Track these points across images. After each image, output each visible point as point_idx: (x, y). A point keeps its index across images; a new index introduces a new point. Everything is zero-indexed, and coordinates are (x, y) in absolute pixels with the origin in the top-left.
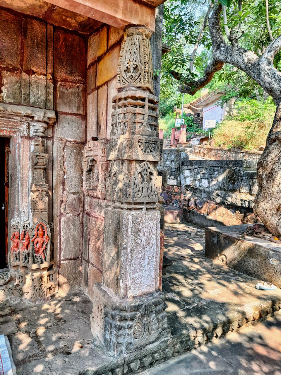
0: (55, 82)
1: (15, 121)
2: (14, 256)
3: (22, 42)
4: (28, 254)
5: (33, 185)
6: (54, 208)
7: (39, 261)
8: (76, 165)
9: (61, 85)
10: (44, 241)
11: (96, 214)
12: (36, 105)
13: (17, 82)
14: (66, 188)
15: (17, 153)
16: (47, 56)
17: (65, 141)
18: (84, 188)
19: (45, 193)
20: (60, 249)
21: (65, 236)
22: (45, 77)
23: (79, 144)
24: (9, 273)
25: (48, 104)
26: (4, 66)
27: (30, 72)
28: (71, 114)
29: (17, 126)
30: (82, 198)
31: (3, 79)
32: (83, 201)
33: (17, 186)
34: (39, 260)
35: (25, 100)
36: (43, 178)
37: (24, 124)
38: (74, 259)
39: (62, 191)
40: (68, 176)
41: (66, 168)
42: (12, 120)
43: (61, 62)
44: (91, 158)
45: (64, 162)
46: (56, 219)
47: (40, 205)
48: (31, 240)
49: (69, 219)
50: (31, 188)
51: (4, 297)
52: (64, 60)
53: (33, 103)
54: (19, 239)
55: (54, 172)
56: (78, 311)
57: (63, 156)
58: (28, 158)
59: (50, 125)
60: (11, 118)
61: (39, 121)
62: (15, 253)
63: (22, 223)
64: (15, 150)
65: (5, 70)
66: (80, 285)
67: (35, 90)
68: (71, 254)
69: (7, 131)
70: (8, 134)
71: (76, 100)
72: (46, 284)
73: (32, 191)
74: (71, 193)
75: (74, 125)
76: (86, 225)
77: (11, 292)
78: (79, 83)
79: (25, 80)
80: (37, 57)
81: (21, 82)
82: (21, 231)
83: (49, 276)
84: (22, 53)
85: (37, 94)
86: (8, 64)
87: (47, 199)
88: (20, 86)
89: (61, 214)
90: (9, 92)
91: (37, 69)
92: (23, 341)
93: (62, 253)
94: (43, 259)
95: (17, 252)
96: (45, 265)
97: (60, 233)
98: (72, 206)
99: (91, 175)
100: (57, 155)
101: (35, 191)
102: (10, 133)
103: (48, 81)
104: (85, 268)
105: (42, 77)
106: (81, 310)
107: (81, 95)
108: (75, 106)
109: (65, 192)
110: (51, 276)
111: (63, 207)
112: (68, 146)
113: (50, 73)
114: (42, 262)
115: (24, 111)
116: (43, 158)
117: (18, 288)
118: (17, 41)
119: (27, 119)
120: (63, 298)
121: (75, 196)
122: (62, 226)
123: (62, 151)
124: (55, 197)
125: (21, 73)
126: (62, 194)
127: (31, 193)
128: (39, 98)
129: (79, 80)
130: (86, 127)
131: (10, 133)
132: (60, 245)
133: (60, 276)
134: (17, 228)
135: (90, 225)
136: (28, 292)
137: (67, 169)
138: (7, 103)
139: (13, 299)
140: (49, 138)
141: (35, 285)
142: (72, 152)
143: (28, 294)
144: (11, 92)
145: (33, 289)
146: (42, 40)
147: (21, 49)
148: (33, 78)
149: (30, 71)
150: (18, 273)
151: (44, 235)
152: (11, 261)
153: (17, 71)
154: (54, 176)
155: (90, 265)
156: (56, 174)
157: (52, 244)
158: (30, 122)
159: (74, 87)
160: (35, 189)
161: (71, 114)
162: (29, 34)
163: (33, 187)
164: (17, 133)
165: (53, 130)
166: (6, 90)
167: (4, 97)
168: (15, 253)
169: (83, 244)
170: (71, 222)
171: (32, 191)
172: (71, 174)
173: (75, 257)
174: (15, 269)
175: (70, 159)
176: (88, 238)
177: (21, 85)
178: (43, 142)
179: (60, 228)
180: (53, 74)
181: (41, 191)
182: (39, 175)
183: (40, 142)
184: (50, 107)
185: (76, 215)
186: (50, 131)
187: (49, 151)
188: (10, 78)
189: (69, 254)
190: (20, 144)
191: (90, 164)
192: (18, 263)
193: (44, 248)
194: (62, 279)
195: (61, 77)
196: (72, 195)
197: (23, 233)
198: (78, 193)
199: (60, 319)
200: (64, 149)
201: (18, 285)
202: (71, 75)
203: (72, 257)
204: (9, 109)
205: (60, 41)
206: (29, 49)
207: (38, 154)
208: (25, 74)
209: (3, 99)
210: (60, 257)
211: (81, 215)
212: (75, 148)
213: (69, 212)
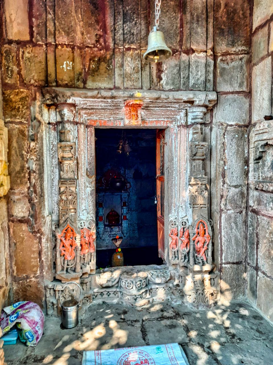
0: (215, 58)
1: (173, 109)
2: (173, 253)
3: (181, 20)
4: (188, 253)
5: (193, 178)
6: (212, 204)
7: (199, 263)
8: (238, 153)
9: (222, 60)
10: (205, 240)
11: (270, 212)
12: (196, 88)
14: (227, 180)
15: (174, 145)
16: (207, 29)
17: (225, 125)
18: (252, 179)
19: (204, 186)
20: (222, 250)
21: (226, 236)
22: (205, 53)
23: (241, 127)
24: (168, 271)
25: (208, 85)
27: (189, 51)
28: (232, 93)
29: (174, 115)
30: (245, 192)
32: (246, 196)
33: (174, 179)
34: (201, 261)
35: (184, 84)
36: (202, 170)
37: (182, 112)
38: (237, 263)
39: (222, 184)
40: (228, 167)
41: (227, 157)
42: (171, 108)
43: (222, 32)
44: (264, 143)
45: (224, 151)
46: (216, 216)
47: (199, 200)
48: (192, 239)
49: (230, 217)
50: (190, 181)
51: (165, 296)
52: (225, 30)
53: (193, 86)
54: (177, 235)
55: (212, 162)
56: (252, 329)
57: (223, 144)
58: (185, 148)
59: (210, 109)
60: (169, 107)
61: (199, 106)
62: (174, 250)
63: (180, 220)
64: (172, 141)
66: (244, 294)
67: (194, 72)
68: (234, 257)
69: (164, 121)
70: (165, 125)
71: (239, 76)
72: (209, 289)
73: (190, 184)
74: (232, 186)
75: (236, 106)
76: (252, 225)
77: (170, 291)
78: (242, 54)
79: (184, 62)
80: (196, 33)
81: (180, 65)
82: (179, 228)
83: (210, 279)
84: (182, 32)
85: (197, 75)
87: (207, 193)
88: (179, 70)
89: (222, 210)
91: (197, 46)
92: (199, 356)
93: (223, 255)
94: (205, 260)
95: (176, 250)
96: (207, 267)
97: (220, 233)
98: (233, 201)
99: (261, 163)
100: (217, 143)
101: (194, 185)
102: (167, 123)
103: (208, 58)
104: (252, 276)
105: (202, 55)
106: (255, 327)
107: (244, 67)
108: (237, 82)
109: (226, 185)
110: (212, 280)
111: (223, 202)
112: (228, 131)
113: (210, 49)
114: (203, 264)
115: (185, 96)
116: (202, 147)
117: (178, 288)
118: (177, 20)
119: (186, 105)
120: (227, 308)
121: (237, 190)
122: (222, 224)
123: (222, 137)
124: (213, 191)
125: (180, 54)
126: (222, 187)
127: (190, 187)
128: (198, 79)
129: (242, 50)
130: (250, 105)
131: (167, 123)
132: (221, 246)
133: (222, 281)
134: (175, 224)
135: (258, 226)
136: (190, 295)
137: (228, 157)
138: (166, 91)
139: (175, 300)
140: (207, 124)
141: (197, 288)
142: (233, 138)
143: (190, 297)
144: (170, 78)
145: (195, 293)
146: (202, 11)
147: (180, 28)
149: (190, 50)
150: (178, 272)
151: (205, 234)
152: (170, 259)
153: (177, 53)
154: (212, 167)
155: (259, 273)
156: (215, 164)
157: (213, 244)
158: (188, 109)
159: (236, 60)
160: (194, 183)
161: (232, 93)
162: (188, 9)
163: (193, 180)
164: (174, 123)
165: (211, 115)
166: (166, 76)
167: (164, 84)
168: (174, 250)
169: (247, 247)
170: (233, 220)
171: (190, 184)
172: (233, 165)
173: (237, 261)
174: (174, 267)
175: (231, 146)
176: (255, 241)
177: (180, 68)
178: (201, 129)
179: (220, 226)
180: (213, 49)
181: (200, 184)
182: (198, 167)
183: (199, 129)
184: (209, 89)
185: (238, 212)
186: (208, 116)
187: (207, 139)
189: (231, 257)
190: (176, 134)
191: (261, 150)
192: (176, 261)
193: (206, 249)
194: (224, 285)
195: (221, 51)
196: (234, 189)
197: (182, 230)
198: (240, 186)
199: (233, 336)
200: (224, 134)
201: (178, 285)
202: (233, 46)
203: (235, 261)
204: (171, 97)
205: (220, 8)
206: (189, 26)
207: (197, 143)
209: (163, 87)
210: (221, 259)
211: (244, 212)
212: (237, 132)
213: (230, 208)
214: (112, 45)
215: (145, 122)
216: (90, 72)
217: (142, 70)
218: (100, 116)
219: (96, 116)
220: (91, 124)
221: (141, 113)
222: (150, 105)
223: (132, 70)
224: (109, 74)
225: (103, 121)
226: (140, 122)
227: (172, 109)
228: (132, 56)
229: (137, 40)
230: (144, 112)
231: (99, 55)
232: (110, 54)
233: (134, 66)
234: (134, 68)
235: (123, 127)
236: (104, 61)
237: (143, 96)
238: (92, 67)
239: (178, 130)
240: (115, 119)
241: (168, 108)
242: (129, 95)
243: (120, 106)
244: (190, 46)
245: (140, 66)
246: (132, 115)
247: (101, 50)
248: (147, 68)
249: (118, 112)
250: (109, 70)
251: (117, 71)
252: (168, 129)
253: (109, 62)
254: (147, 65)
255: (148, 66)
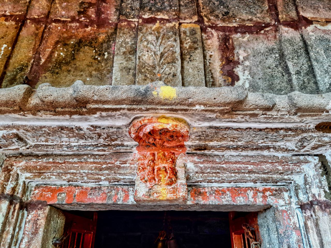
1: (280, 155)
13: (271, 51)
26: (235, 25)
31: (235, 52)
37: (307, 162)
42: (273, 153)
60: (268, 148)
65: (236, 32)
69: (256, 191)
70: (260, 201)
79: (291, 42)
86: (244, 20)
90: (257, 77)
131: (265, 197)
148: (311, 34)
153: (267, 29)
164: (286, 195)
166: (247, 73)
188: (252, 45)
208: (286, 29)
214: (113, 18)
215: (200, 194)
216: (50, 65)
217: (183, 59)
218: (69, 176)
219: (59, 175)
220: (42, 199)
221: (185, 166)
222: (211, 144)
223: (158, 57)
224: (97, 70)
225: (77, 191)
226: (182, 192)
227: (276, 154)
228: (159, 33)
229: (170, 6)
230: (195, 163)
231: (81, 35)
232: (107, 33)
233: (162, 50)
234: (162, 55)
235: (133, 205)
236: (90, 45)
237: (183, 96)
238: (59, 55)
239: (307, 219)
240: (115, 184)
241: (266, 153)
242: (131, 95)
243: (123, 145)
244: (298, 13)
245: (178, 50)
246: (159, 169)
247: (87, 26)
248: (198, 55)
249: (118, 163)
250: (99, 62)
251: (119, 62)
252: (269, 214)
253: (102, 49)
254: (196, 49)
255: (200, 51)
